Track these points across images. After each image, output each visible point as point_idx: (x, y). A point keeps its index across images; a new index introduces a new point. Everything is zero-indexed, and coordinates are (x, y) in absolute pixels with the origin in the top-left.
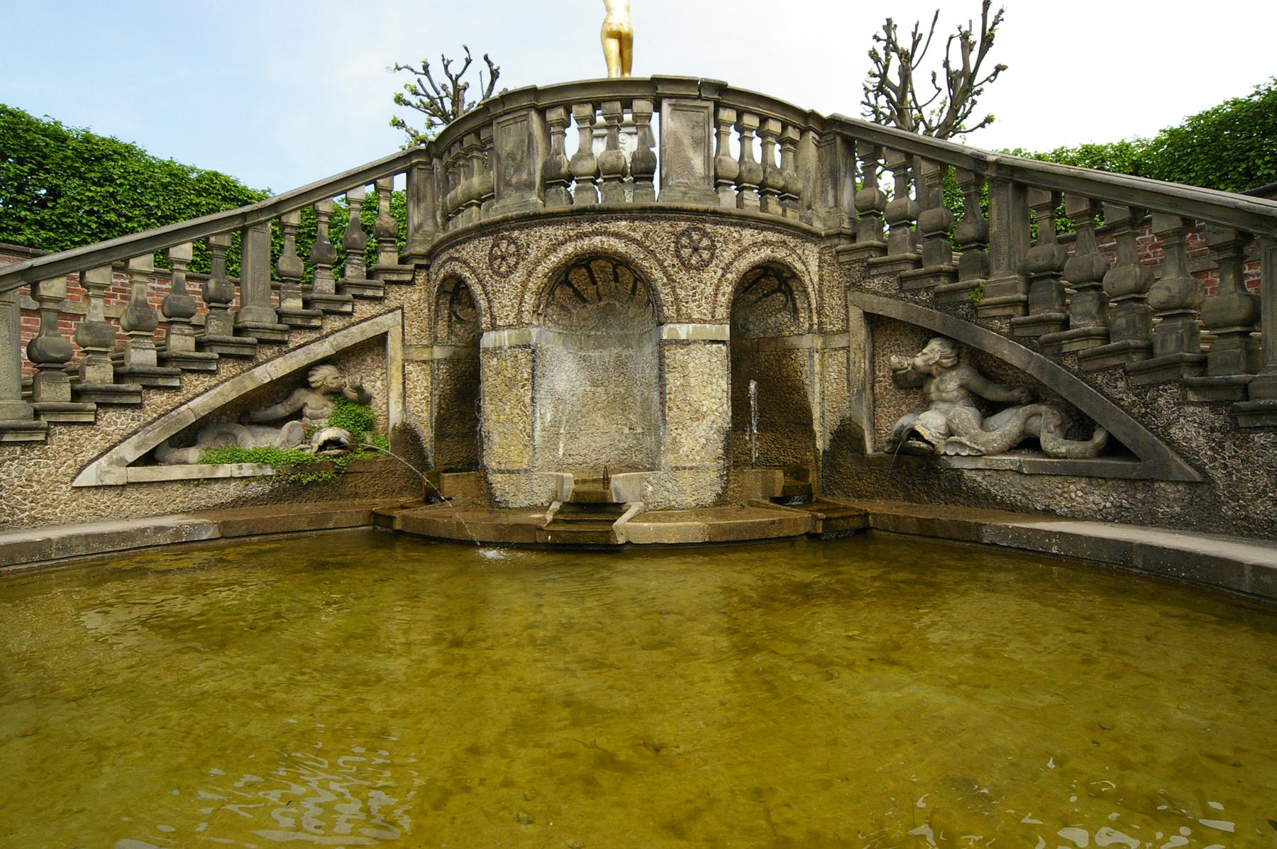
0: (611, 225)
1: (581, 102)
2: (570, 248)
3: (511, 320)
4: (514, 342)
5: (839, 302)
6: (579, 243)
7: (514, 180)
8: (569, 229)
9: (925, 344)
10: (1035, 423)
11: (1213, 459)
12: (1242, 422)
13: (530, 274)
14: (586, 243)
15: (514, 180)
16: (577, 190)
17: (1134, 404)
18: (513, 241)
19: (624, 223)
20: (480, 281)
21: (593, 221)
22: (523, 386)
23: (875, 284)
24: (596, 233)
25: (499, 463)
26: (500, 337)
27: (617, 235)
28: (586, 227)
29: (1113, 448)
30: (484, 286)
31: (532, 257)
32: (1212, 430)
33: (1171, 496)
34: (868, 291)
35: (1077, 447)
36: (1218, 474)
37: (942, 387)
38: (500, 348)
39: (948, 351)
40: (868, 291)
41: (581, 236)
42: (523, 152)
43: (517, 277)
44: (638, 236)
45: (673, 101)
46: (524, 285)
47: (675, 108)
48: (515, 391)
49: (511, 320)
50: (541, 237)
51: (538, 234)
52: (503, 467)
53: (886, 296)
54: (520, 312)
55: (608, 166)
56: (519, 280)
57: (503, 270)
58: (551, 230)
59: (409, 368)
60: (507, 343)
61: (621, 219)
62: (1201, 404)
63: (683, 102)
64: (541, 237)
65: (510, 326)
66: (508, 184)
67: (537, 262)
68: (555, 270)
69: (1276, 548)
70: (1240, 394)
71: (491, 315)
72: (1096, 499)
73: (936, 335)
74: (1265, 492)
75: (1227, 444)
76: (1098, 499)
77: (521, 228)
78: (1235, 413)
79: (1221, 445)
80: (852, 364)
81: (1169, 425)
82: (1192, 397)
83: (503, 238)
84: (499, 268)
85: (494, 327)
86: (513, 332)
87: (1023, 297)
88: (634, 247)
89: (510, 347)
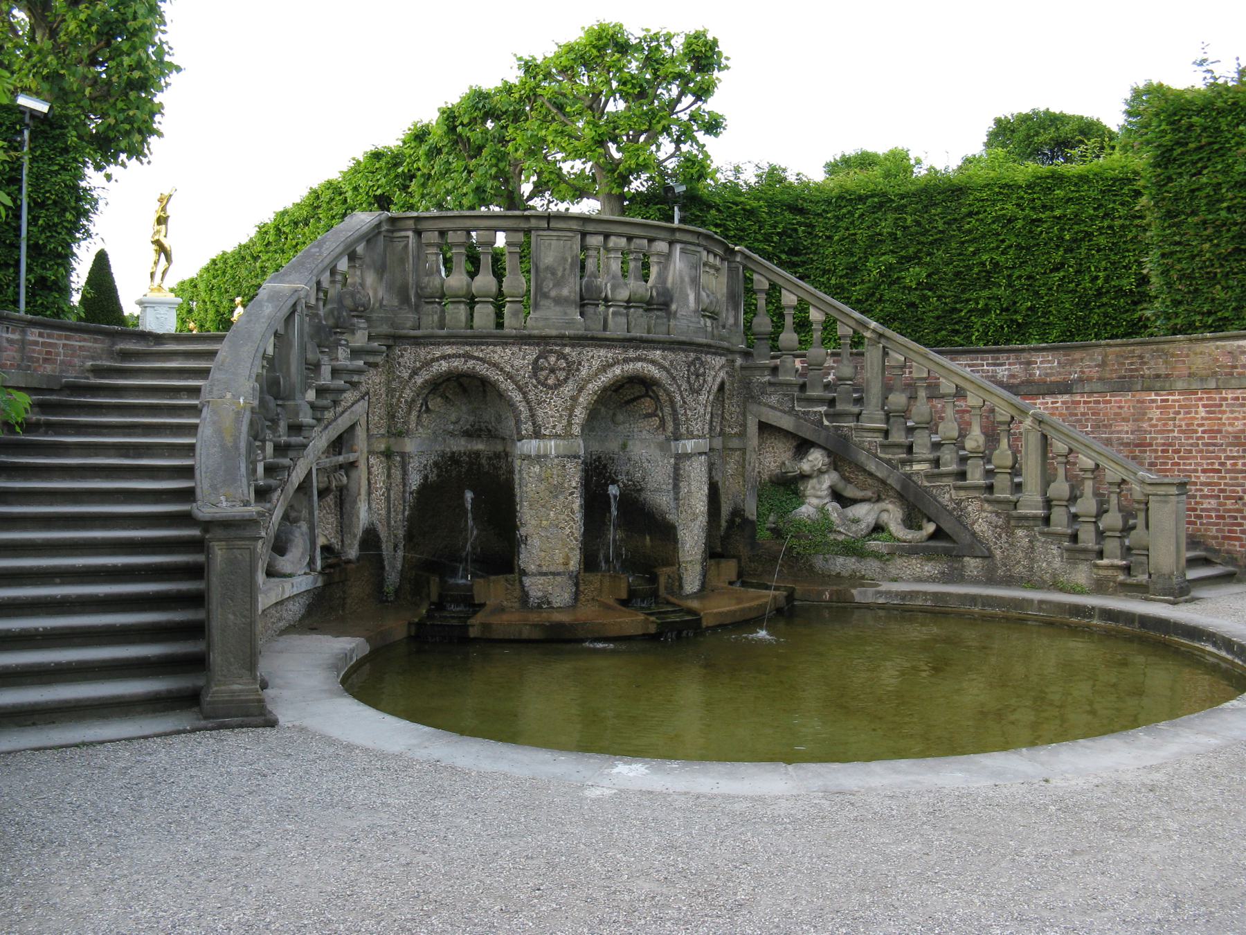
0: (649, 353)
1: (619, 235)
2: (617, 371)
3: (559, 430)
4: (561, 452)
5: (738, 410)
6: (626, 367)
7: (553, 293)
8: (618, 353)
9: (806, 453)
10: (885, 516)
11: (996, 544)
12: (1013, 523)
13: (581, 390)
14: (630, 368)
15: (553, 293)
16: (614, 314)
17: (954, 509)
18: (564, 357)
19: (658, 352)
20: (520, 389)
21: (637, 348)
22: (572, 494)
23: (773, 400)
24: (639, 359)
25: (540, 566)
26: (545, 446)
27: (653, 362)
28: (632, 354)
29: (938, 534)
30: (525, 394)
31: (584, 372)
32: (996, 527)
33: (972, 565)
34: (766, 405)
35: (909, 535)
36: (998, 553)
37: (817, 486)
38: (546, 456)
39: (827, 460)
40: (766, 405)
41: (626, 361)
42: (564, 270)
43: (568, 390)
44: (667, 364)
45: (683, 246)
46: (574, 399)
47: (683, 251)
48: (561, 498)
49: (559, 430)
50: (593, 357)
51: (590, 354)
52: (544, 569)
53: (781, 411)
54: (570, 424)
55: (638, 296)
56: (570, 394)
57: (550, 382)
58: (602, 352)
59: (372, 461)
60: (553, 452)
61: (657, 349)
62: (991, 512)
63: (690, 247)
64: (593, 357)
65: (557, 436)
66: (546, 296)
67: (588, 381)
68: (605, 390)
69: (3, 667)
70: (1012, 506)
71: (534, 424)
72: (929, 568)
73: (819, 446)
74: (1019, 562)
75: (1003, 535)
76: (930, 569)
77: (573, 346)
78: (1009, 518)
79: (1000, 535)
80: (747, 463)
81: (974, 523)
82: (986, 505)
83: (551, 351)
84: (546, 379)
85: (537, 435)
86: (561, 442)
87: (884, 426)
88: (665, 373)
89: (557, 457)
